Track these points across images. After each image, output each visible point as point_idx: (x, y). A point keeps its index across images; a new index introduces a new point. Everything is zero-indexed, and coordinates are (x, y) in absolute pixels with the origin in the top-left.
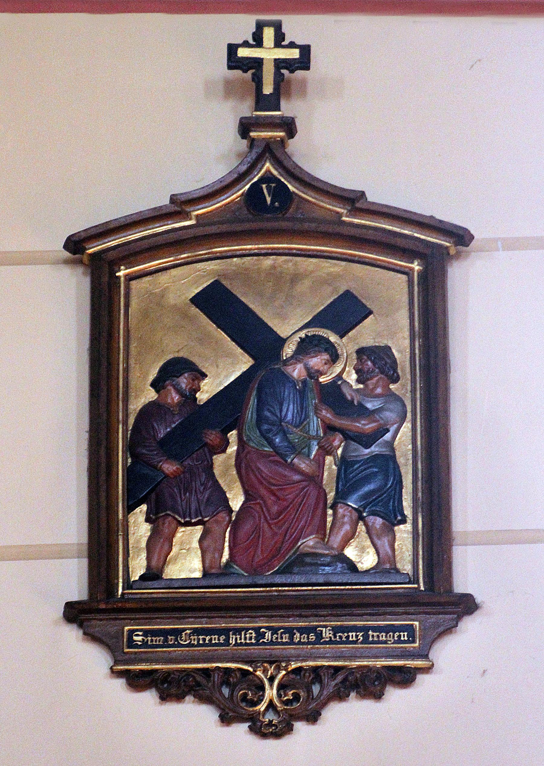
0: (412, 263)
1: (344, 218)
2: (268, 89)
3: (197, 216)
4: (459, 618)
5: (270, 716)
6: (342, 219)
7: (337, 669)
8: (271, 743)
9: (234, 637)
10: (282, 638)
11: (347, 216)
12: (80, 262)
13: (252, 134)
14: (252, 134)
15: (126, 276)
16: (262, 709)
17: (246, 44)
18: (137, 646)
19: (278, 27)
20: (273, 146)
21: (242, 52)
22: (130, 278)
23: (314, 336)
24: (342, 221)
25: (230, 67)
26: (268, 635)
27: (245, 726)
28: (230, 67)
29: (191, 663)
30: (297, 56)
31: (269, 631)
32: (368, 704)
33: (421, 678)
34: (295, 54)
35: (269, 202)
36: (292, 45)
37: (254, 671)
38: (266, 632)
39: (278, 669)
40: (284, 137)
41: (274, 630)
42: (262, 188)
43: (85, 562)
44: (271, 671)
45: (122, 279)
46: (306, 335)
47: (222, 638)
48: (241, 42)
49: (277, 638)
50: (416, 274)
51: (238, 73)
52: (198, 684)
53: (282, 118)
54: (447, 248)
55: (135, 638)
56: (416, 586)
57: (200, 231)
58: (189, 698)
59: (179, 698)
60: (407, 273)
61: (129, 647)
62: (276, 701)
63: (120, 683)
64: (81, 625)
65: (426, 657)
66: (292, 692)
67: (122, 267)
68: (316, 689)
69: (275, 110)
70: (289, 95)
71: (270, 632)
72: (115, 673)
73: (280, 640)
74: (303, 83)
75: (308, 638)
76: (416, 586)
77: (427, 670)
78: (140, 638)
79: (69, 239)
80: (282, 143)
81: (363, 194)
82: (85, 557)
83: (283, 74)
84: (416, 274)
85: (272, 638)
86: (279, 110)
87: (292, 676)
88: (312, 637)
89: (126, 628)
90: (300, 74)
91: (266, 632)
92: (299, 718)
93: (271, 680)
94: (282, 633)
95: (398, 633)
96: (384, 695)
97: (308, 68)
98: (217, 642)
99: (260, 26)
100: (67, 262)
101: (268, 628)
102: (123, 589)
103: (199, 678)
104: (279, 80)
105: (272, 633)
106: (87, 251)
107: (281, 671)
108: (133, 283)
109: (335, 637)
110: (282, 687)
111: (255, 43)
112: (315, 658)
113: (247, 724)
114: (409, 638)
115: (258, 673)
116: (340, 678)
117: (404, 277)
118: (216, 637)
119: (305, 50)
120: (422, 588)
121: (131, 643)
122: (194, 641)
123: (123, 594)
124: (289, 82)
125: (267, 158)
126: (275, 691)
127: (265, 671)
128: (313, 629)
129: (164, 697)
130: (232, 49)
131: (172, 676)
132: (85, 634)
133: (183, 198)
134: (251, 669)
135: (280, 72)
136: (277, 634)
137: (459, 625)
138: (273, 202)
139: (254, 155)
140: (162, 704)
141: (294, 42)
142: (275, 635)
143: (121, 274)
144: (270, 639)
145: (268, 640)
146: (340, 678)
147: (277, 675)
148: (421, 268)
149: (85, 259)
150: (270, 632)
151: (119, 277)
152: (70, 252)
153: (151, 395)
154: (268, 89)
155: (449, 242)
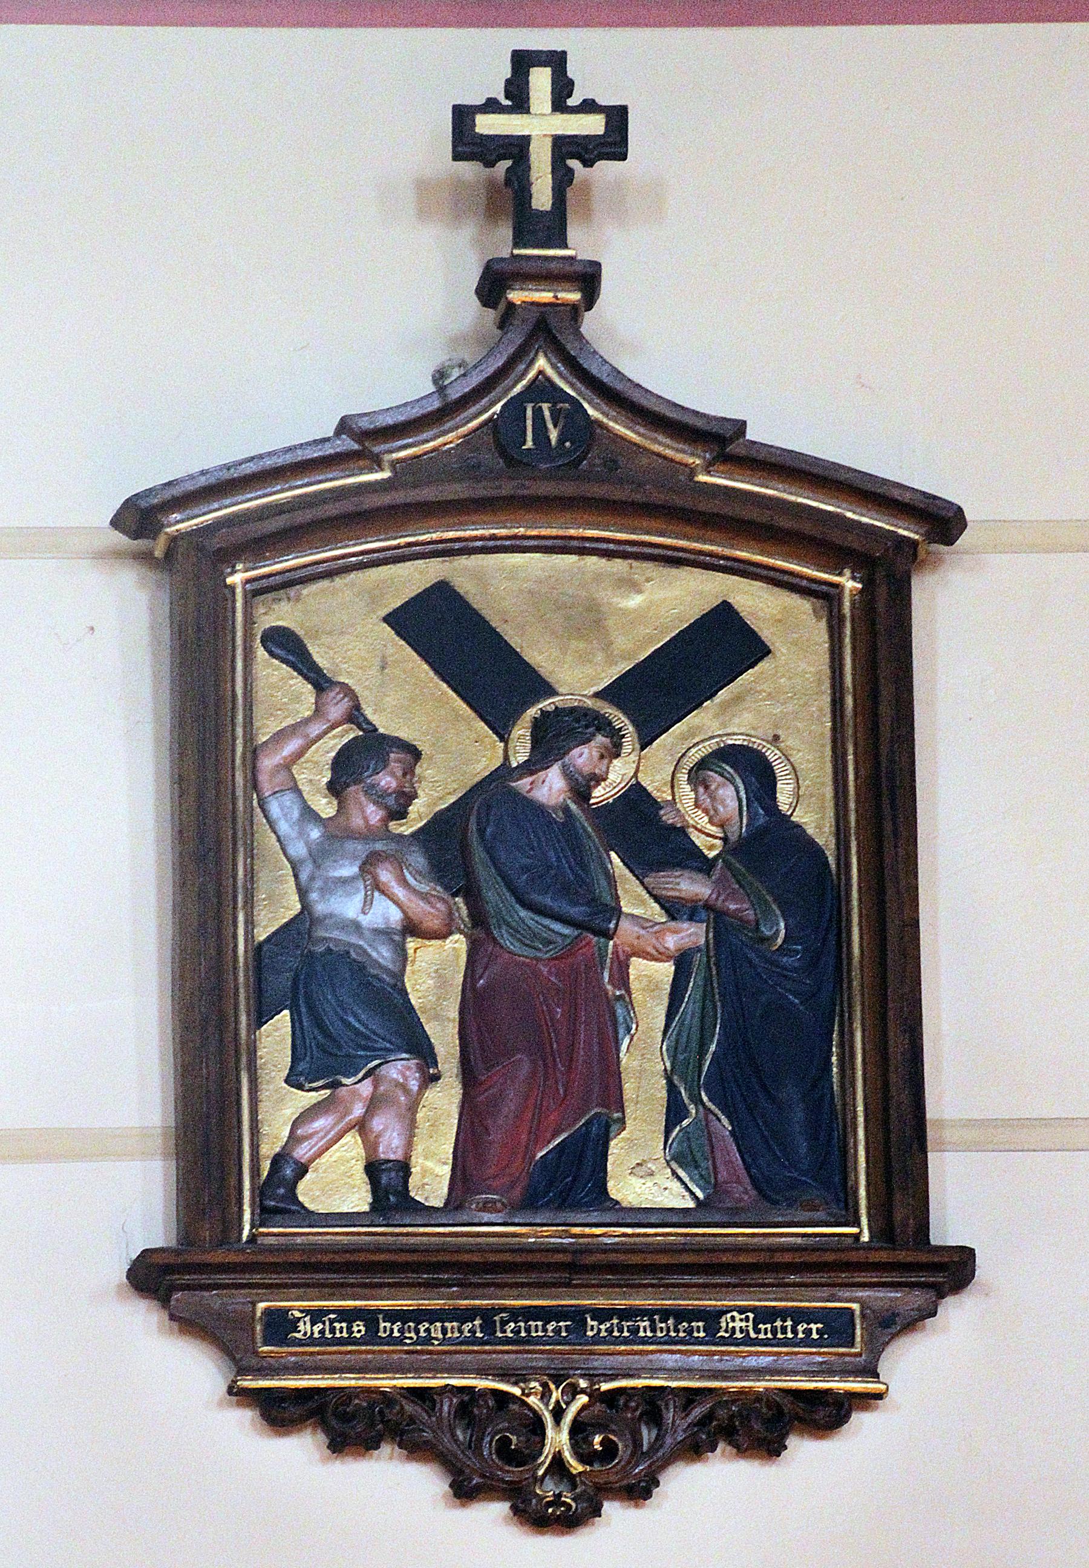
0: (840, 574)
1: (702, 478)
3: (393, 464)
4: (942, 1296)
5: (549, 1489)
6: (696, 479)
7: (691, 1397)
9: (663, 1325)
10: (333, 1330)
12: (145, 558)
13: (516, 296)
14: (516, 296)
16: (541, 1472)
17: (491, 106)
19: (557, 61)
20: (553, 322)
21: (487, 125)
22: (258, 590)
24: (697, 482)
25: (457, 157)
28: (457, 157)
33: (858, 1419)
34: (593, 125)
36: (589, 106)
37: (523, 1394)
39: (574, 1391)
40: (701, 473)
41: (317, 1316)
43: (929, 1115)
45: (239, 591)
48: (480, 101)
49: (322, 1332)
50: (847, 604)
51: (470, 170)
54: (914, 544)
56: (854, 1230)
58: (386, 1449)
59: (366, 1444)
62: (567, 1455)
63: (247, 1416)
64: (164, 1301)
65: (871, 1372)
67: (239, 566)
68: (647, 1435)
72: (238, 1394)
75: (350, 1331)
76: (854, 1230)
80: (575, 313)
81: (740, 427)
82: (145, 1155)
83: (571, 171)
84: (847, 604)
86: (565, 246)
87: (598, 1407)
88: (359, 1329)
89: (262, 1306)
90: (606, 168)
93: (558, 1414)
94: (332, 1322)
95: (512, 1325)
96: (785, 1448)
97: (623, 157)
99: (522, 61)
100: (117, 554)
101: (306, 1311)
104: (562, 179)
106: (168, 530)
107: (578, 1396)
110: (577, 1429)
111: (510, 103)
112: (653, 1372)
114: (821, 1337)
115: (533, 1400)
116: (697, 1412)
118: (344, 1325)
119: (618, 117)
120: (865, 1238)
122: (385, 1327)
123: (252, 1239)
124: (586, 186)
125: (540, 347)
126: (564, 1436)
127: (545, 1395)
130: (463, 116)
131: (357, 1401)
132: (172, 1317)
133: (365, 424)
134: (517, 1391)
135: (565, 165)
136: (324, 1323)
137: (940, 1310)
138: (561, 441)
139: (516, 338)
142: (684, 1324)
143: (236, 579)
144: (309, 1334)
145: (305, 1334)
146: (697, 1412)
147: (568, 1404)
150: (307, 1319)
151: (232, 588)
154: (542, 197)
155: (916, 533)
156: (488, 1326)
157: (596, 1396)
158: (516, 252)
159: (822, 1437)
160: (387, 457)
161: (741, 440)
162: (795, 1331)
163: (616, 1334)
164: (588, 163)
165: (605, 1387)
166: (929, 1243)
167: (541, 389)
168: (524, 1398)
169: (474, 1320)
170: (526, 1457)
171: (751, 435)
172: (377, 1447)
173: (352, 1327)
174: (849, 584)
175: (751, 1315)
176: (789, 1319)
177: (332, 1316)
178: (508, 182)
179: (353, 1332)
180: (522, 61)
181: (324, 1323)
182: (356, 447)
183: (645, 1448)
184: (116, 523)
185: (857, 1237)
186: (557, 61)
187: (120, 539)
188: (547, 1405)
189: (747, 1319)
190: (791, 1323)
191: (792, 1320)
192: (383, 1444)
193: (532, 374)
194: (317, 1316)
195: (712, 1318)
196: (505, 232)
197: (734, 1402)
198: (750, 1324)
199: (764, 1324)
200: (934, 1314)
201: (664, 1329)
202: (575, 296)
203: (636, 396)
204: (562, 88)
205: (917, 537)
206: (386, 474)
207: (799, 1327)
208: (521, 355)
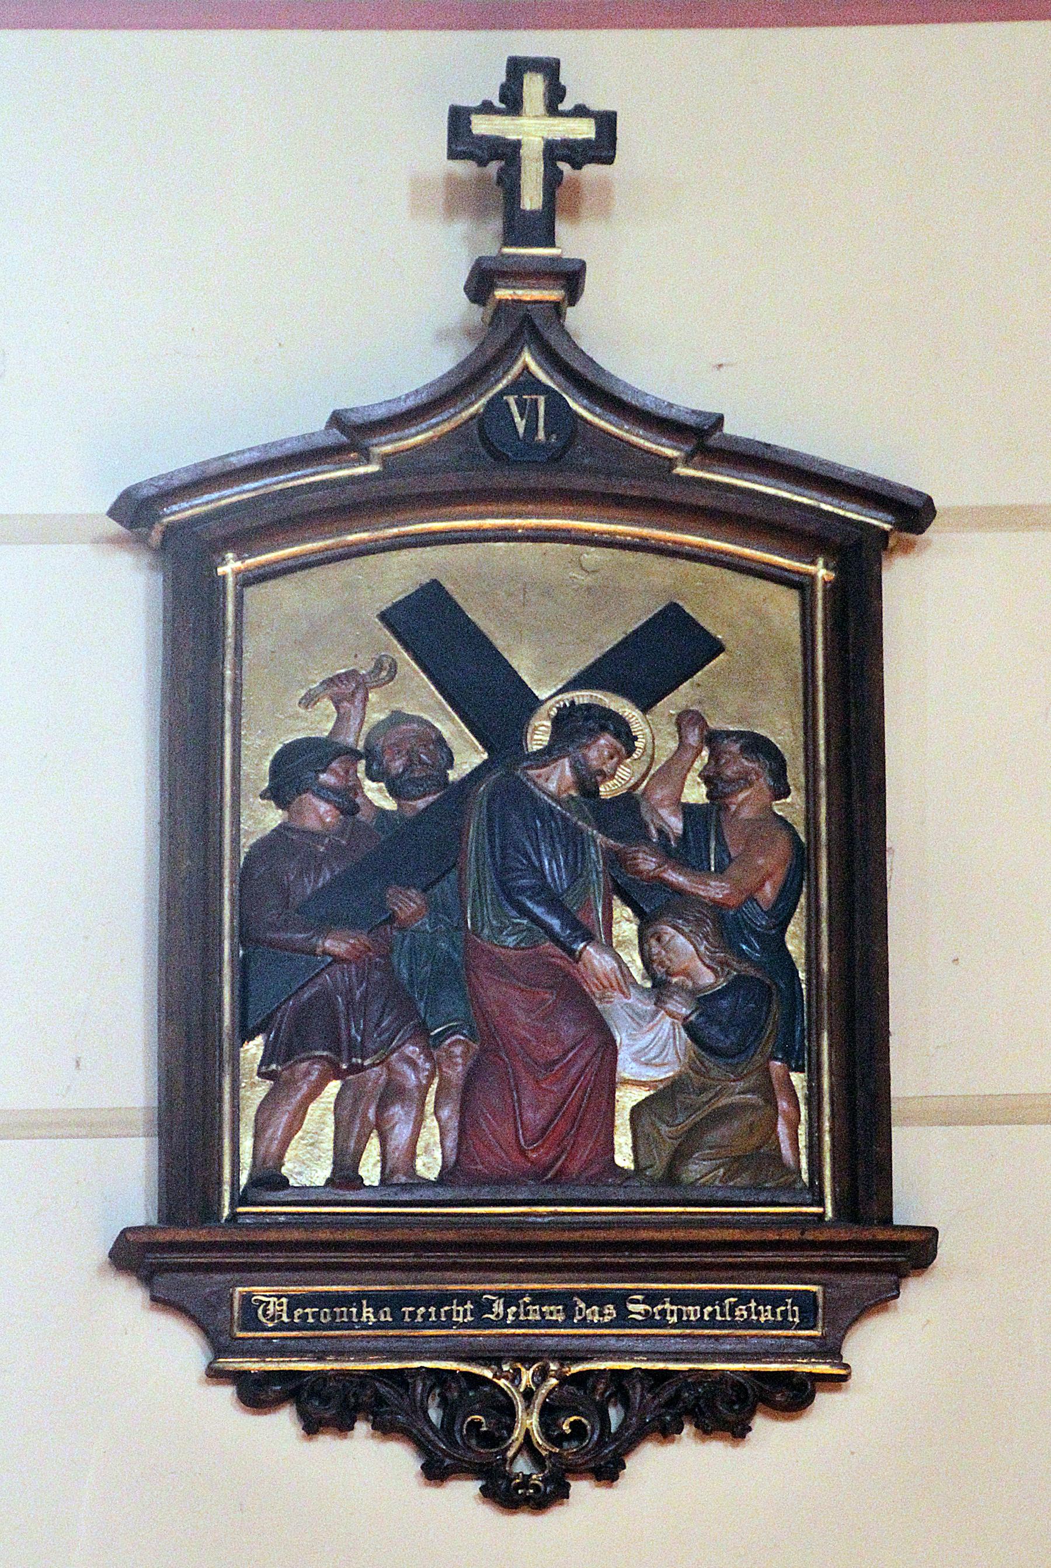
0: (813, 563)
1: (682, 471)
2: (532, 199)
4: (905, 1276)
8: (523, 1521)
9: (461, 1309)
11: (687, 462)
13: (502, 294)
14: (502, 294)
15: (237, 573)
17: (487, 108)
18: (636, 1324)
19: (550, 69)
21: (482, 126)
22: (249, 580)
23: (588, 707)
25: (453, 155)
26: (498, 1308)
27: (473, 1487)
28: (453, 155)
29: (412, 1359)
30: (592, 135)
31: (499, 1298)
32: (717, 1449)
33: (823, 1400)
34: (584, 130)
35: (521, 430)
36: (581, 111)
37: (495, 1376)
38: (494, 1301)
41: (511, 1299)
42: (507, 404)
44: (527, 1377)
45: (230, 580)
46: (572, 703)
47: (610, 1309)
49: (516, 1314)
51: (464, 168)
52: (380, 1401)
53: (554, 259)
54: (885, 534)
55: (631, 1307)
56: (821, 1210)
57: (398, 486)
59: (344, 1427)
60: (802, 585)
61: (244, 1328)
62: (537, 1438)
63: (227, 1393)
65: (831, 1351)
66: (572, 1419)
68: (615, 1415)
69: (546, 246)
70: (574, 213)
71: (502, 1300)
72: (215, 1375)
73: (522, 1318)
74: (605, 188)
76: (821, 1210)
77: (837, 1381)
78: (641, 1308)
79: (126, 496)
80: (557, 310)
83: (561, 172)
85: (506, 1315)
86: (552, 244)
88: (610, 1309)
90: (591, 171)
91: (494, 1301)
92: (579, 1472)
95: (709, 1309)
96: (750, 1429)
97: (609, 160)
98: (460, 1320)
99: (517, 68)
100: (115, 541)
101: (499, 1294)
102: (233, 1205)
103: (383, 1390)
104: (552, 182)
105: (504, 1303)
108: (249, 592)
109: (291, 1315)
110: (549, 1414)
113: (479, 1484)
115: (502, 1383)
116: (665, 1396)
117: (795, 594)
119: (607, 122)
121: (251, 1321)
123: (234, 1216)
124: (576, 188)
126: (535, 1416)
128: (475, 1298)
129: (312, 1427)
130: (459, 118)
132: (154, 1299)
133: (356, 419)
134: (488, 1374)
136: (518, 1307)
139: (503, 336)
140: (311, 1439)
141: (584, 106)
142: (298, 1310)
144: (501, 1317)
147: (538, 1386)
148: (832, 575)
149: (156, 537)
150: (502, 1300)
152: (120, 522)
153: (273, 817)
154: (532, 199)
156: (569, 1311)
157: (564, 1380)
158: (507, 250)
159: (791, 1419)
160: (377, 450)
161: (718, 433)
162: (438, 1316)
163: (719, 1318)
164: (577, 166)
165: (575, 1369)
166: (890, 1219)
167: (527, 383)
168: (495, 1380)
169: (466, 1304)
170: (495, 1439)
171: (729, 428)
172: (352, 1429)
173: (735, 1312)
174: (821, 572)
175: (284, 1300)
176: (469, 1302)
177: (527, 1299)
178: (500, 181)
179: (735, 1316)
180: (517, 68)
181: (518, 1307)
182: (344, 439)
183: (613, 1430)
184: (113, 513)
185: (824, 1213)
186: (550, 69)
187: (114, 527)
188: (517, 1387)
189: (281, 1305)
190: (755, 1304)
191: (755, 1301)
192: (357, 1425)
193: (516, 369)
194: (511, 1299)
195: (621, 1300)
196: (496, 224)
197: (701, 1383)
198: (285, 1308)
199: (694, 1306)
200: (897, 1296)
201: (461, 1313)
202: (554, 295)
203: (618, 391)
204: (555, 94)
205: (887, 527)
206: (373, 468)
207: (705, 1310)
208: (506, 354)
